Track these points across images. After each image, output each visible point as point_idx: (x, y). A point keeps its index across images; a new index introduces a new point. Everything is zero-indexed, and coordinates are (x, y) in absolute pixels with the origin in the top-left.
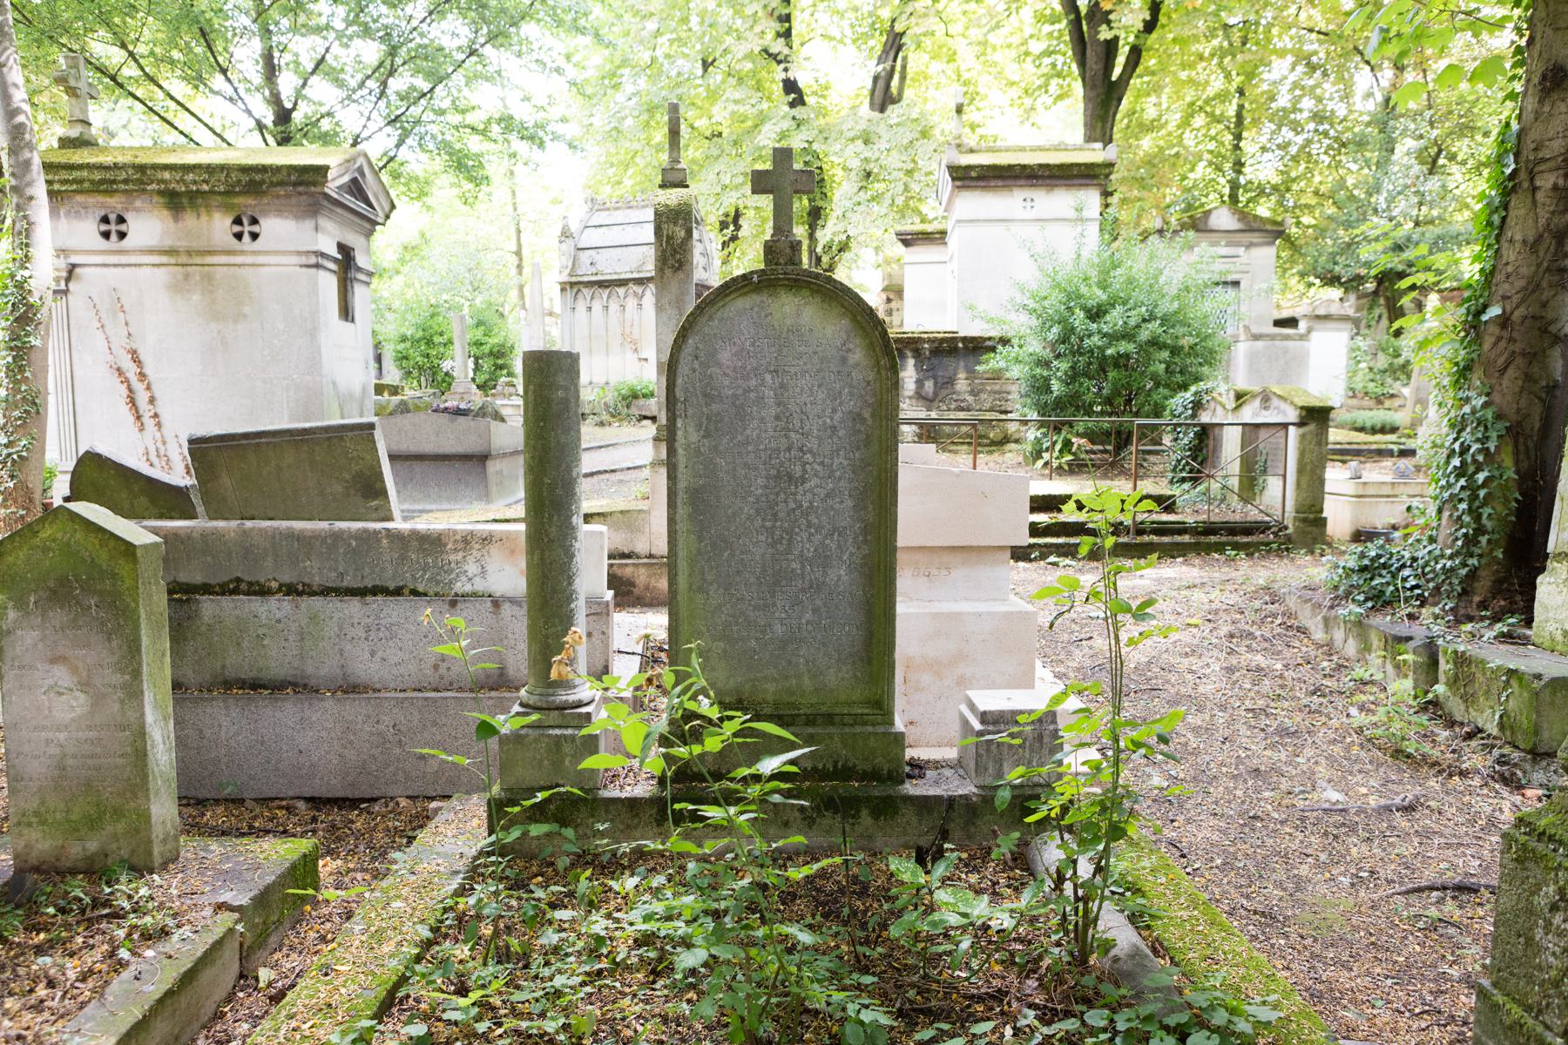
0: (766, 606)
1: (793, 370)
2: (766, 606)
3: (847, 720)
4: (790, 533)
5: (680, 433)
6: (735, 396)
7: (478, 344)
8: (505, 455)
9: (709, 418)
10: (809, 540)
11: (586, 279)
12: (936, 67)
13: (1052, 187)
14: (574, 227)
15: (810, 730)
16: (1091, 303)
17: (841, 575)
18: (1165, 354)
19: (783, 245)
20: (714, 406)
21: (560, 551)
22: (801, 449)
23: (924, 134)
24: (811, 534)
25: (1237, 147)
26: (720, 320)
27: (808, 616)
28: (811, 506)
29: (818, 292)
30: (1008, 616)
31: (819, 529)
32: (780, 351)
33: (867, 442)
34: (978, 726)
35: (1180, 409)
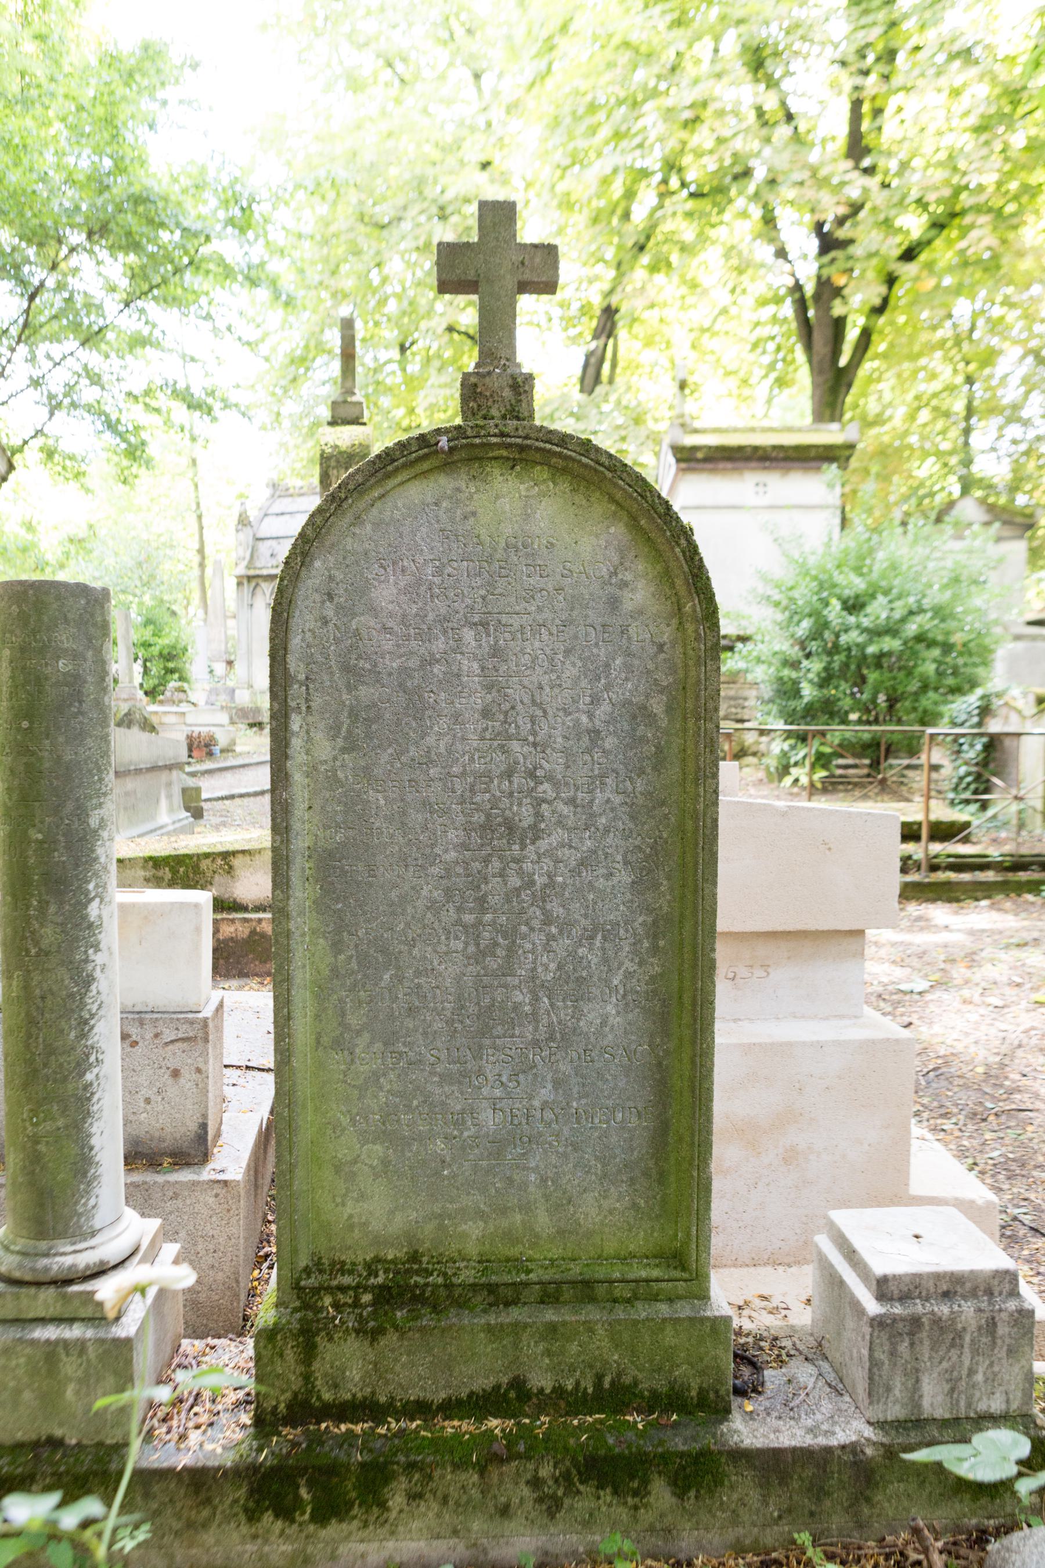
0: (464, 1074)
1: (516, 622)
2: (464, 1074)
3: (619, 1290)
4: (511, 934)
5: (296, 743)
6: (404, 670)
7: (147, 645)
8: (138, 771)
9: (354, 715)
10: (547, 949)
11: (265, 572)
12: (648, 356)
13: (788, 470)
14: (253, 514)
15: (550, 1315)
16: (847, 593)
17: (610, 1017)
18: (936, 652)
19: (498, 382)
20: (363, 691)
21: (62, 972)
22: (532, 774)
23: (638, 421)
24: (551, 938)
25: (966, 444)
26: (376, 525)
27: (546, 1093)
28: (551, 884)
29: (564, 471)
30: (869, 1046)
31: (566, 926)
32: (491, 585)
33: (659, 761)
34: (873, 1307)
35: (963, 717)
